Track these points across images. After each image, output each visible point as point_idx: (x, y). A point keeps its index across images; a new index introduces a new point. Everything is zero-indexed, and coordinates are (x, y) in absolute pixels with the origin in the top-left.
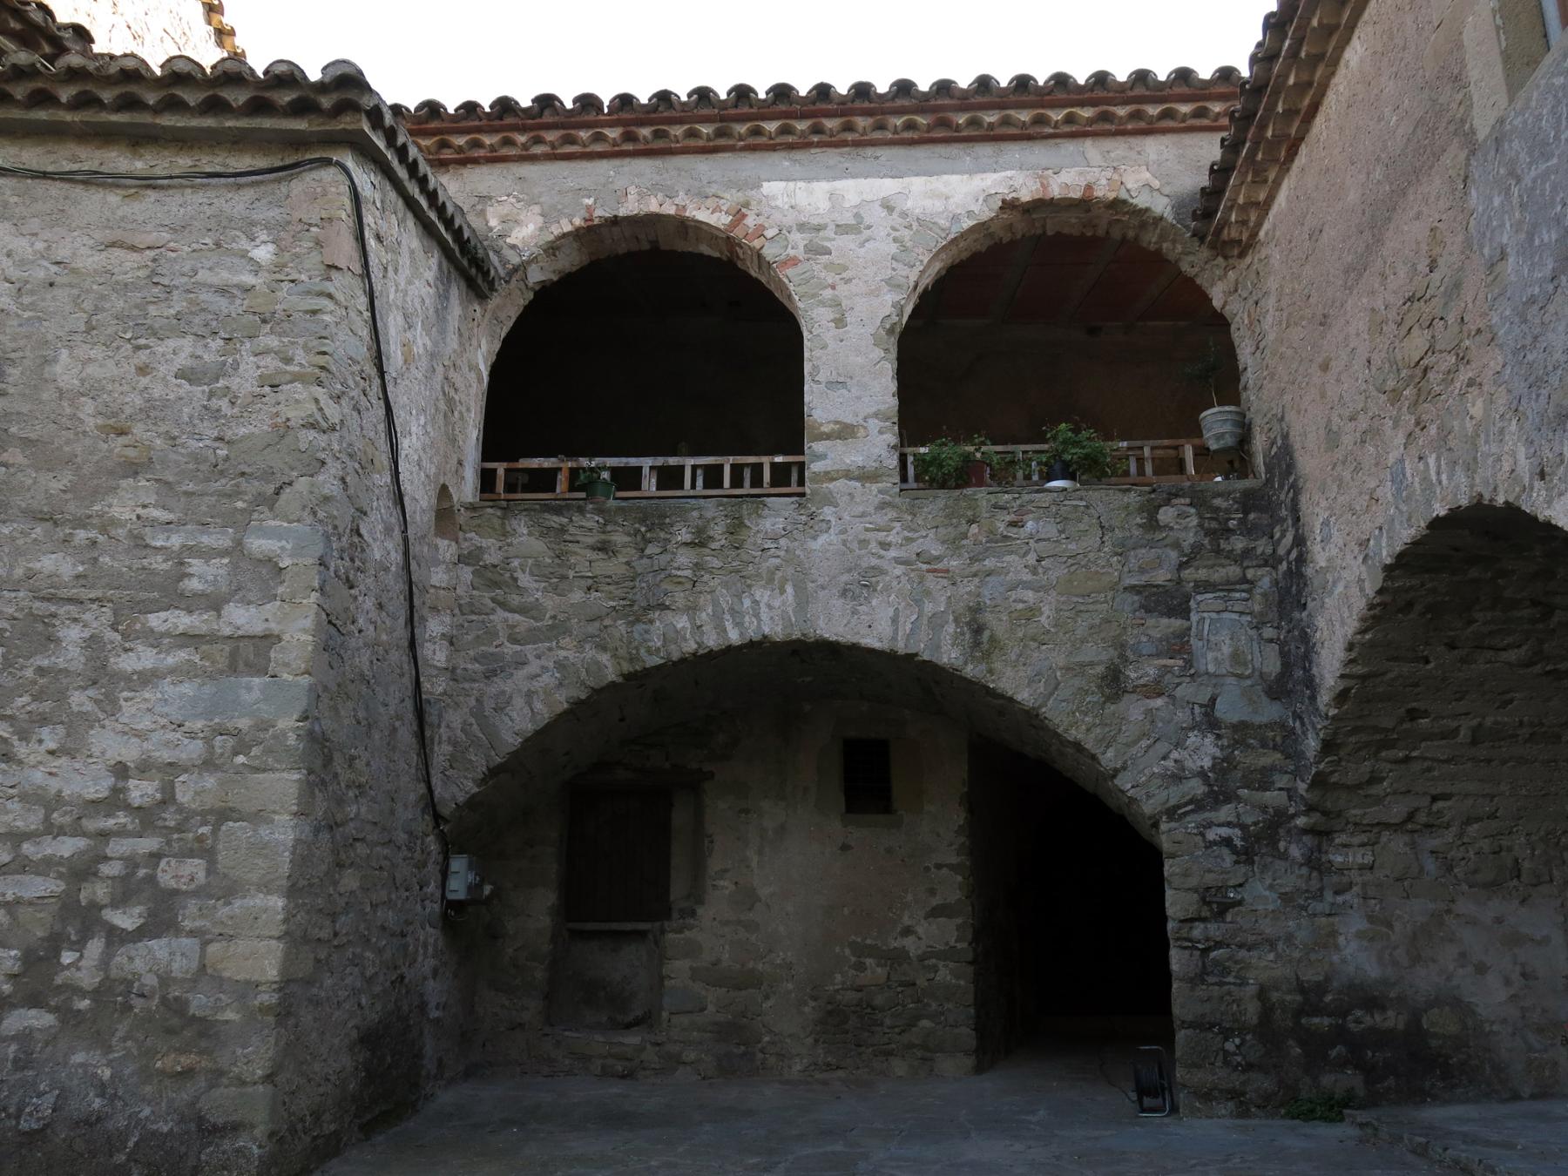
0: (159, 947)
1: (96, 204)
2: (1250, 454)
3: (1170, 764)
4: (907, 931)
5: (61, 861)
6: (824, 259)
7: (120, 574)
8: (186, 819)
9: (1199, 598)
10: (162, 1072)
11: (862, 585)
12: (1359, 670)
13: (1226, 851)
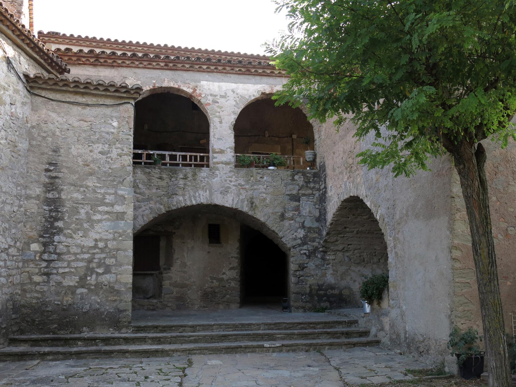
0: (108, 276)
1: (76, 109)
3: (294, 236)
4: (224, 274)
5: (85, 259)
6: (217, 104)
7: (92, 198)
8: (110, 251)
9: (303, 198)
10: (110, 300)
11: (225, 191)
12: (335, 219)
13: (305, 256)
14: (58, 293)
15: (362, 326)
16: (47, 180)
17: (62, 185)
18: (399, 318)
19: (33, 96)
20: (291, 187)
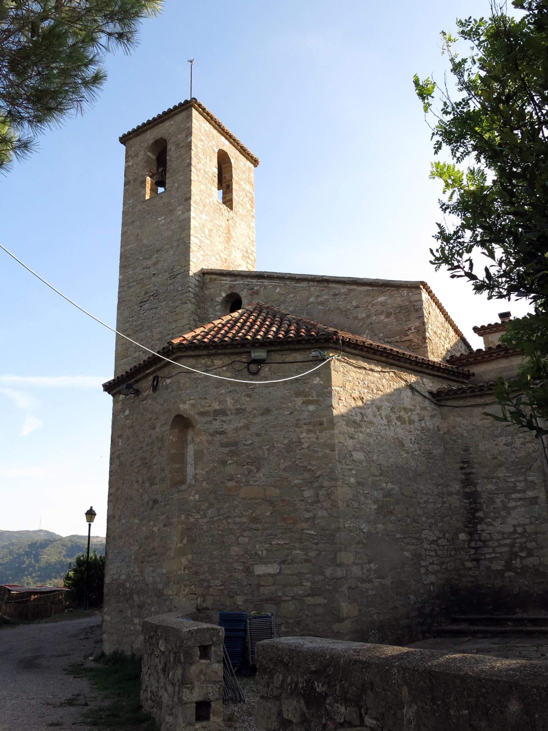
0: (531, 559)
16: (463, 477)
17: (476, 479)
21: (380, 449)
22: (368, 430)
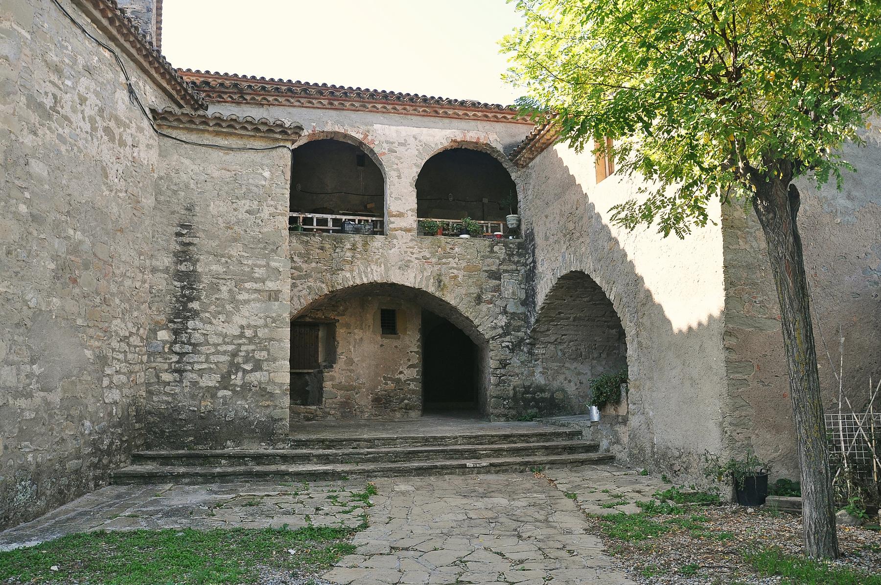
0: (258, 374)
1: (216, 155)
2: (520, 230)
3: (493, 324)
4: (401, 373)
10: (262, 406)
11: (405, 266)
12: (548, 302)
14: (193, 397)
15: (587, 438)
16: (178, 248)
18: (644, 427)
19: (161, 137)
20: (490, 261)
21: (74, 170)
22: (60, 131)
